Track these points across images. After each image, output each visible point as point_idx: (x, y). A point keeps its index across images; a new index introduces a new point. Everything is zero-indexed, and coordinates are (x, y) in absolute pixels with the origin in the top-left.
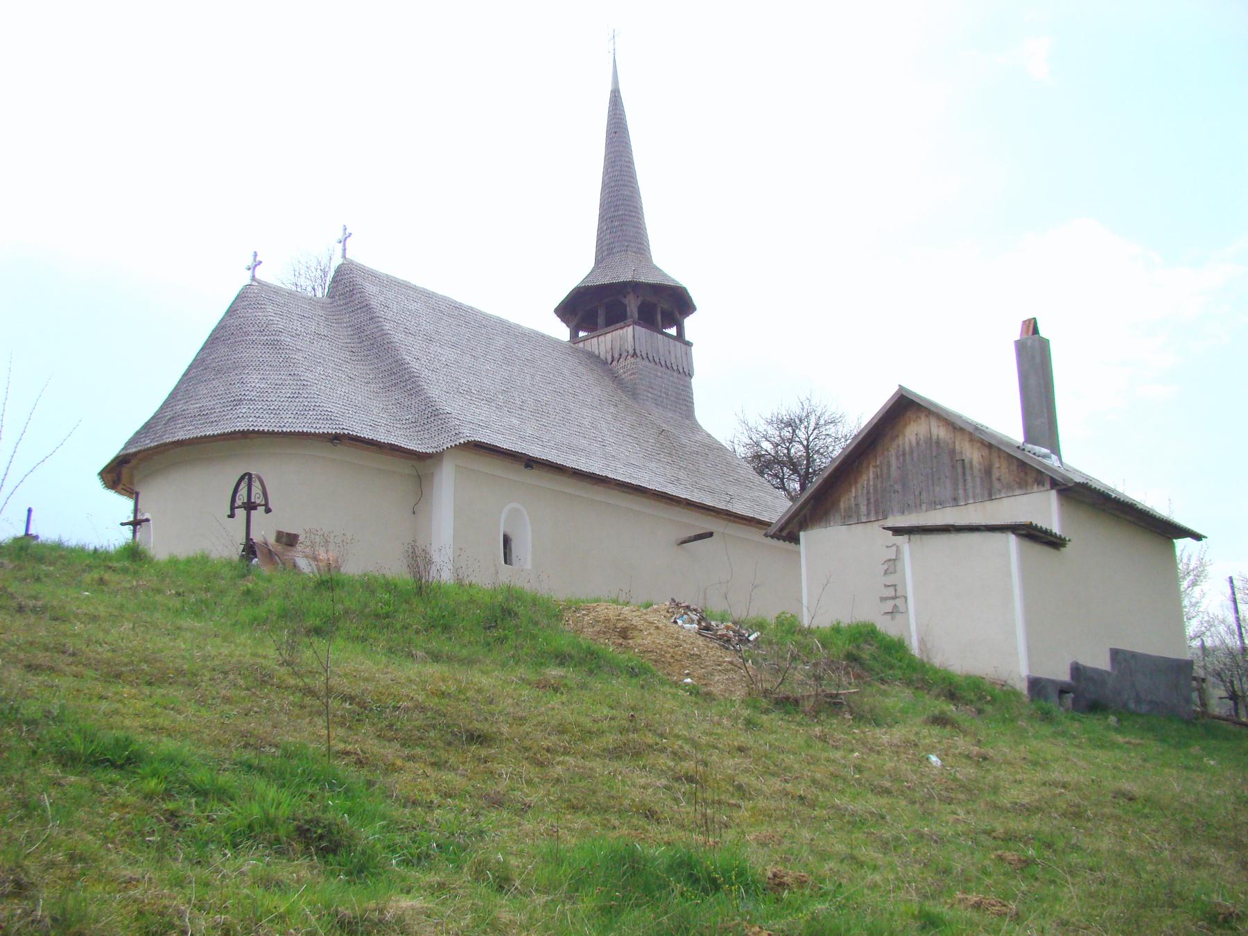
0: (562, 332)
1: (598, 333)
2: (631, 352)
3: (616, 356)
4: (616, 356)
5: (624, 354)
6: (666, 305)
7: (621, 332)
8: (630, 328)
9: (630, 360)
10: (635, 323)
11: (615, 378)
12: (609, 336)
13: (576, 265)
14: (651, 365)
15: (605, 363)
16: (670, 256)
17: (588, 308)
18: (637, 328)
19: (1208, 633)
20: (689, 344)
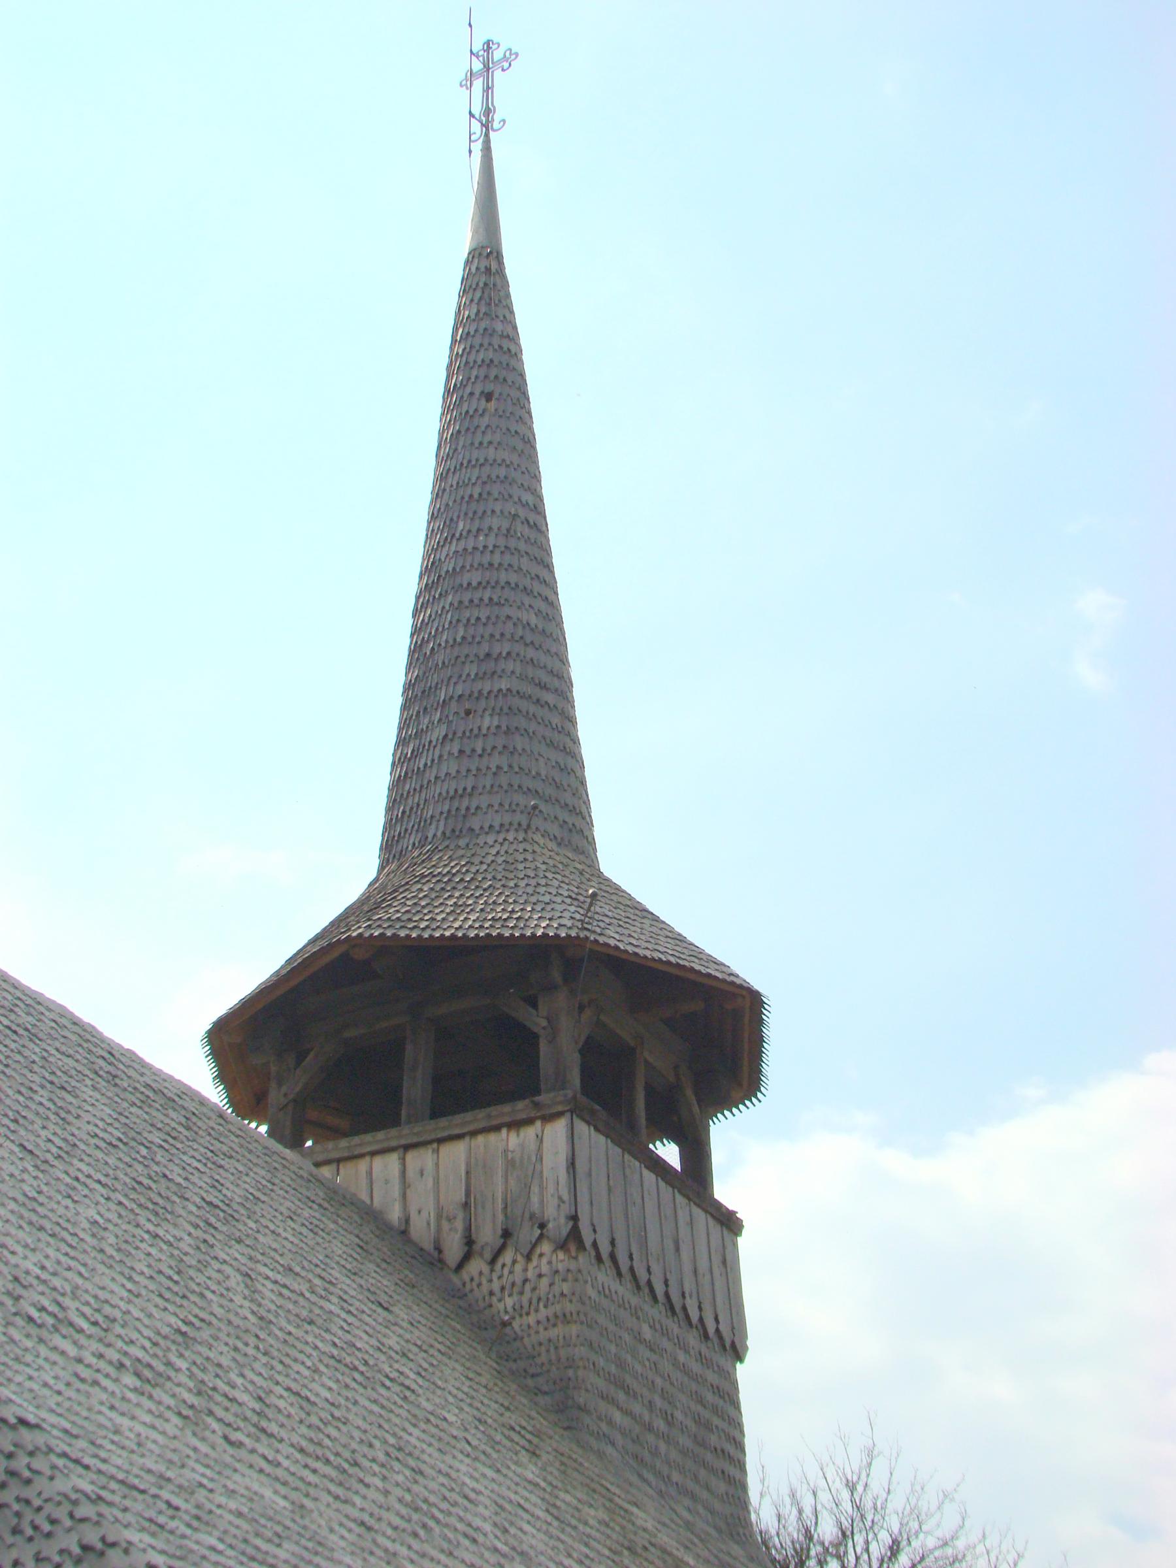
0: (199, 1075)
1: (405, 1133)
2: (559, 1226)
3: (487, 1235)
4: (487, 1235)
5: (527, 1234)
6: (684, 1041)
7: (513, 1140)
8: (557, 1131)
9: (548, 1258)
10: (576, 1110)
11: (493, 1337)
12: (456, 1154)
13: (290, 852)
14: (623, 1290)
15: (433, 1259)
16: (673, 839)
17: (350, 1038)
18: (582, 1127)
19: (980, 1548)
20: (729, 1223)
